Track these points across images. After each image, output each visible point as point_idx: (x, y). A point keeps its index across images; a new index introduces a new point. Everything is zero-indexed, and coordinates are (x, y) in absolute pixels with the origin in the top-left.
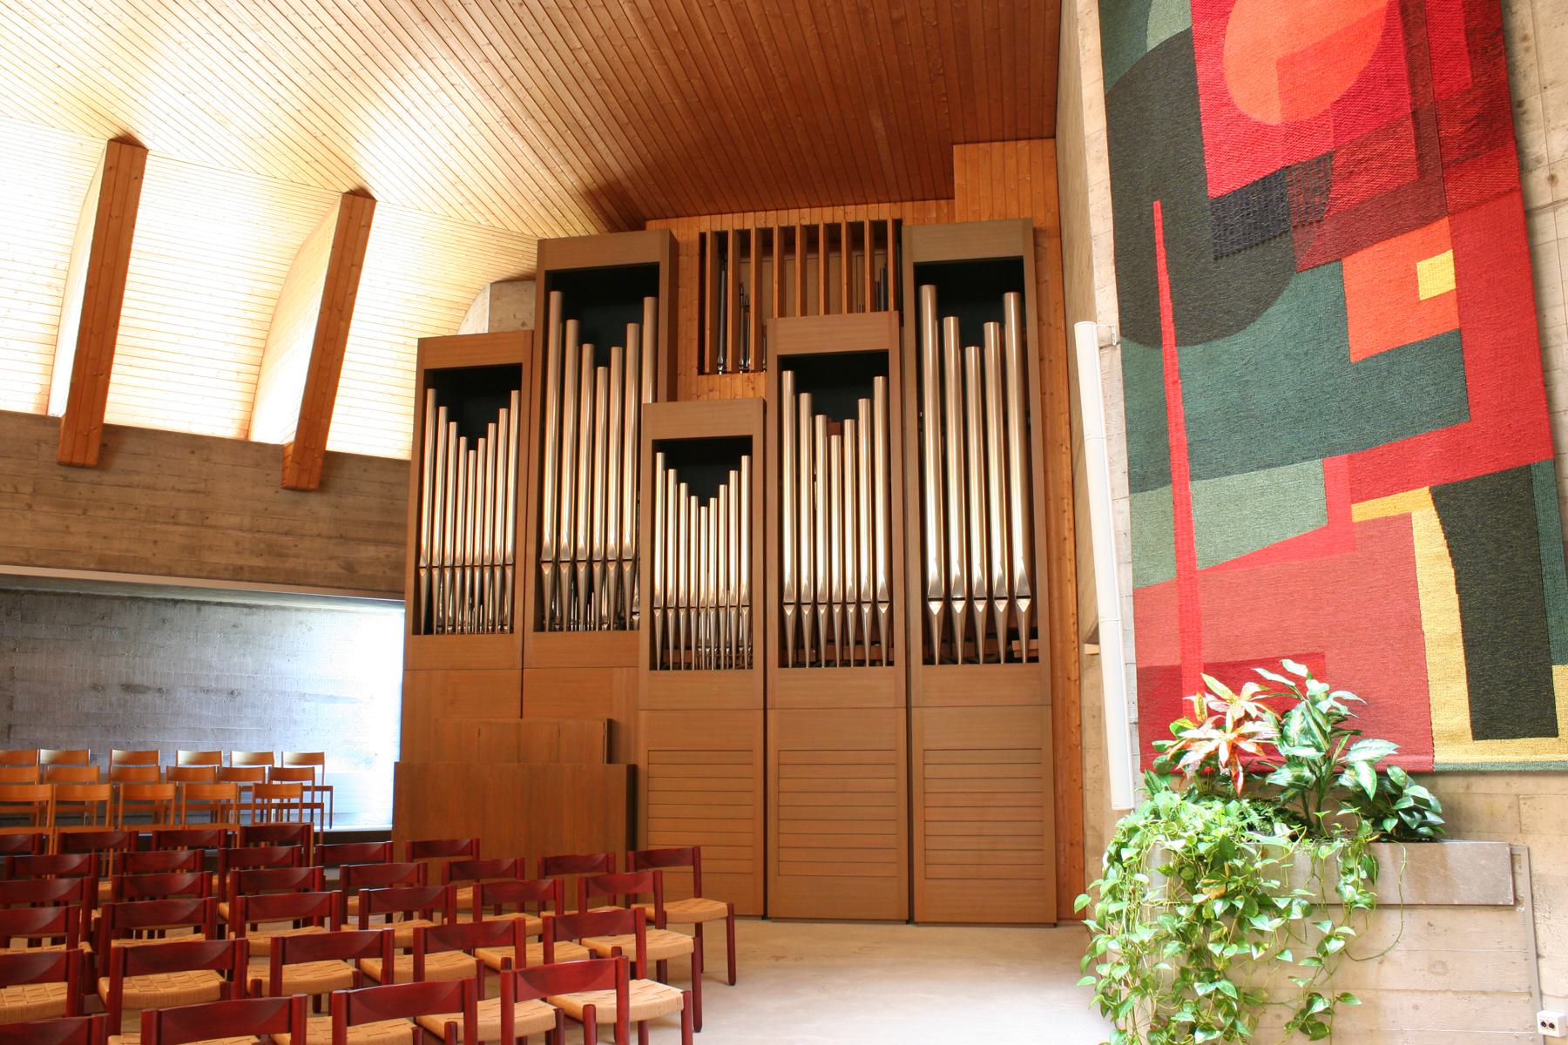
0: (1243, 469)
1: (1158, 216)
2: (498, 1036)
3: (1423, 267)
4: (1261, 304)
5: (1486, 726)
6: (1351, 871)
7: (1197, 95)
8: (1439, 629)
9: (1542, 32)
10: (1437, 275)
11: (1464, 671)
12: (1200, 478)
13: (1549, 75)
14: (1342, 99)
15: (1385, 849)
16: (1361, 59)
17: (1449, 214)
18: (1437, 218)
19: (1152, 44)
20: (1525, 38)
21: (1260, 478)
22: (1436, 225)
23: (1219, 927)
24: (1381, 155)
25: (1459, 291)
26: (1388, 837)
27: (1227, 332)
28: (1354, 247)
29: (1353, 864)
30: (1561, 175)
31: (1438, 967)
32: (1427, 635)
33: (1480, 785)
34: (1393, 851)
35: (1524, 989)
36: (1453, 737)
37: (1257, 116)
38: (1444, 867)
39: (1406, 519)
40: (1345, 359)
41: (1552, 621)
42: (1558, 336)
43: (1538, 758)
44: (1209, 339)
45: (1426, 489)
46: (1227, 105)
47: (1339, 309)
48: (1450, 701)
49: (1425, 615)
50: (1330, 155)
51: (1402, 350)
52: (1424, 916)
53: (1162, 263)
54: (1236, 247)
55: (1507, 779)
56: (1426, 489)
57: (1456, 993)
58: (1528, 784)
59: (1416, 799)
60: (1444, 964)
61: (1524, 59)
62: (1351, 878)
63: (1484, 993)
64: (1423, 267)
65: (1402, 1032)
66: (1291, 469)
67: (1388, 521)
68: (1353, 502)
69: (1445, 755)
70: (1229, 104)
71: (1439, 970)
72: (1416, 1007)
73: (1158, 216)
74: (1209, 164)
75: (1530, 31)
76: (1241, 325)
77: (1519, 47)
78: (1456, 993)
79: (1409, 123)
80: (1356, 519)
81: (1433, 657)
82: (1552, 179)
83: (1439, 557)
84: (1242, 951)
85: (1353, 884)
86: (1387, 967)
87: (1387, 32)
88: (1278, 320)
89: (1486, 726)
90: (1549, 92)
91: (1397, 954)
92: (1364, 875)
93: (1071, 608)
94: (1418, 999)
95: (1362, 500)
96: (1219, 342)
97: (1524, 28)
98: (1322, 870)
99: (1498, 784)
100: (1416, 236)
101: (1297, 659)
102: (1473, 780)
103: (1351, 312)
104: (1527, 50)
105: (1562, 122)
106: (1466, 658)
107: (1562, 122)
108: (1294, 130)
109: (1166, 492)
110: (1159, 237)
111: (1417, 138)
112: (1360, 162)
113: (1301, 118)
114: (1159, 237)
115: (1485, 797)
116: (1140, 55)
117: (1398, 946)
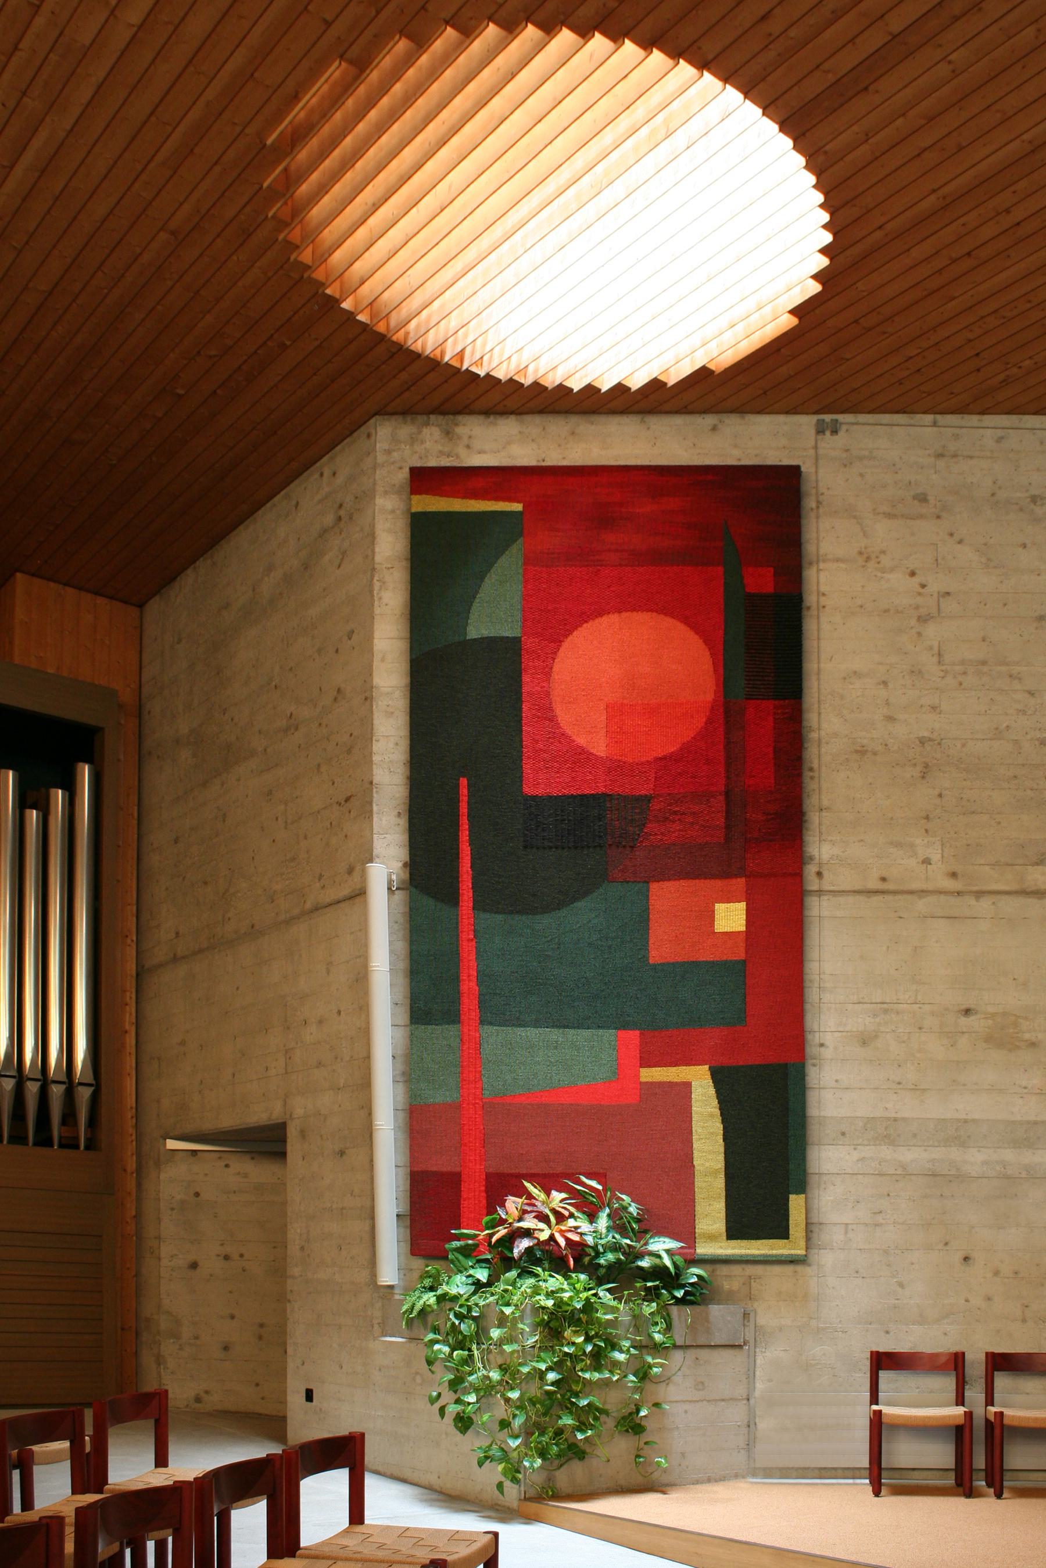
0: (536, 1024)
1: (464, 791)
2: (171, 1440)
3: (720, 908)
4: (566, 898)
5: (735, 1231)
6: (657, 1324)
7: (519, 700)
8: (707, 1164)
9: (824, 769)
10: (731, 917)
11: (724, 1194)
12: (491, 1024)
13: (825, 803)
14: (664, 758)
15: (674, 1310)
16: (685, 732)
17: (746, 876)
18: (736, 876)
19: (473, 632)
20: (811, 769)
21: (555, 1035)
22: (734, 881)
23: (583, 1360)
24: (694, 813)
25: (747, 932)
26: (679, 1302)
27: (532, 911)
28: (663, 876)
29: (658, 1319)
30: (825, 873)
31: (700, 1385)
32: (697, 1168)
33: (723, 1270)
34: (679, 1311)
35: (745, 1396)
36: (711, 1238)
37: (581, 740)
38: (708, 1321)
39: (688, 1085)
40: (645, 958)
41: (792, 1166)
42: (811, 981)
43: (774, 1252)
44: (511, 912)
45: (707, 1067)
46: (551, 720)
47: (643, 921)
48: (711, 1212)
49: (696, 1154)
50: (648, 799)
51: (696, 964)
52: (692, 1354)
53: (464, 835)
54: (546, 843)
55: (744, 1266)
56: (707, 1067)
57: (709, 1401)
58: (759, 1269)
59: (698, 1276)
60: (702, 1383)
61: (810, 785)
62: (658, 1328)
63: (723, 1400)
64: (720, 908)
65: (678, 1428)
66: (586, 1033)
67: (671, 1085)
68: (641, 1066)
69: (703, 1249)
70: (553, 719)
71: (700, 1387)
72: (686, 1412)
73: (464, 791)
74: (527, 767)
75: (815, 766)
76: (546, 909)
77: (807, 774)
78: (709, 1401)
79: (722, 798)
80: (643, 1079)
81: (700, 1183)
82: (819, 874)
83: (712, 1115)
84: (602, 1376)
85: (659, 1332)
86: (671, 1387)
87: (709, 721)
88: (585, 916)
89: (735, 1231)
90: (824, 814)
91: (678, 1379)
92: (664, 1326)
93: (131, 1101)
94: (687, 1406)
95: (649, 1066)
96: (524, 917)
97: (811, 763)
98: (638, 1323)
99: (736, 1270)
100: (718, 883)
101: (589, 1176)
102: (718, 1266)
103: (653, 925)
104: (812, 778)
105: (830, 838)
106: (726, 1185)
107: (830, 838)
108: (615, 767)
109: (451, 1032)
110: (464, 808)
111: (727, 812)
112: (675, 813)
113: (624, 759)
114: (464, 808)
115: (730, 1280)
116: (462, 638)
117: (679, 1373)
